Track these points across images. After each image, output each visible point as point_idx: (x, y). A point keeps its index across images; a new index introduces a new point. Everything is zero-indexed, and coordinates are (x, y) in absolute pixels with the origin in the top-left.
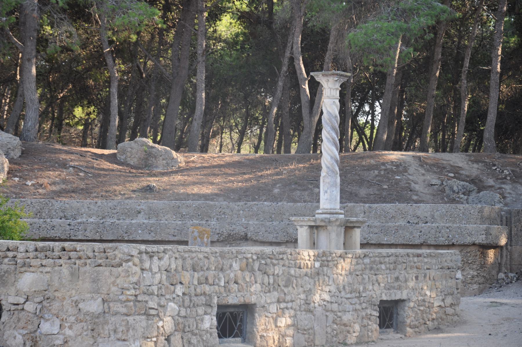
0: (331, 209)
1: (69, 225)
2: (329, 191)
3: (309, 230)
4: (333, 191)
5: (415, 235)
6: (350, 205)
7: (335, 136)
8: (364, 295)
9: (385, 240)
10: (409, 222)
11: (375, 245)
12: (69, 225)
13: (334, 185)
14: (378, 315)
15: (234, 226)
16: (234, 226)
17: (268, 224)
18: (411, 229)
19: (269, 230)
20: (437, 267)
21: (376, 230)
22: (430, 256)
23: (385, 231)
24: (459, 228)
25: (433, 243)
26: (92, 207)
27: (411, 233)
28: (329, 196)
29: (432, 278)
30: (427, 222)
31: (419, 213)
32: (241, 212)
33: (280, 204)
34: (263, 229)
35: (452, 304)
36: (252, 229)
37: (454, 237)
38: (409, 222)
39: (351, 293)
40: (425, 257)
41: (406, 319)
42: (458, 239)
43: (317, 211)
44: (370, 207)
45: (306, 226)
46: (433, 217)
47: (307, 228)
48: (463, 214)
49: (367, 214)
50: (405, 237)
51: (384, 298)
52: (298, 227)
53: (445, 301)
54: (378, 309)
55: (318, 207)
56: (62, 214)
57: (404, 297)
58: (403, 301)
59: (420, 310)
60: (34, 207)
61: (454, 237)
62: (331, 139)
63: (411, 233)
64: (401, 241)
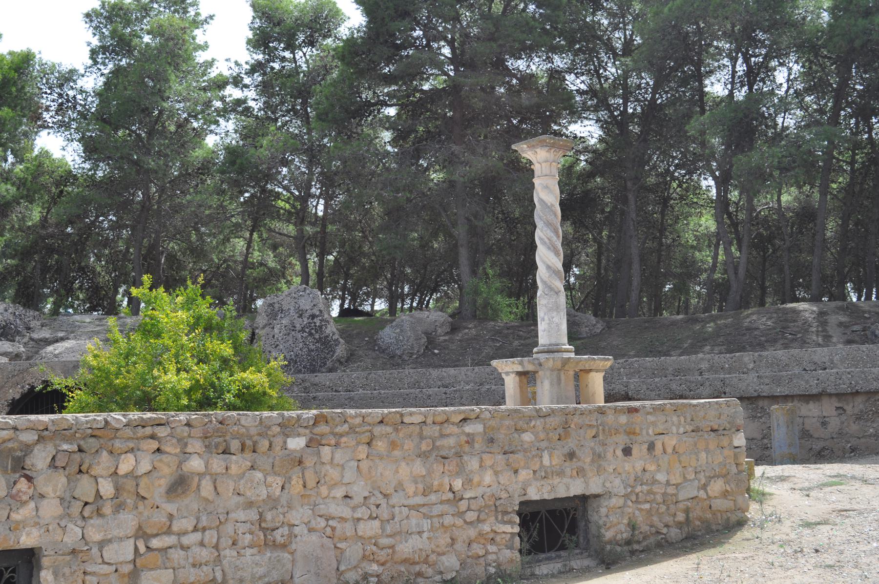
0: (550, 345)
1: (445, 393)
2: (546, 318)
3: (517, 378)
4: (553, 318)
5: (812, 384)
6: (737, 354)
7: (555, 238)
8: (467, 495)
9: (778, 391)
10: (805, 370)
11: (768, 397)
12: (445, 393)
13: (557, 308)
14: (517, 529)
15: (613, 386)
16: (613, 386)
17: (649, 380)
18: (807, 378)
19: (650, 388)
20: (682, 430)
21: (767, 381)
22: (655, 409)
23: (777, 381)
24: (862, 372)
25: (833, 391)
26: (469, 373)
27: (807, 382)
28: (552, 322)
29: (669, 450)
30: (825, 369)
31: (816, 358)
32: (622, 370)
33: (663, 358)
34: (645, 387)
35: (727, 491)
36: (632, 387)
37: (857, 383)
38: (805, 370)
39: (424, 494)
40: (648, 413)
41: (603, 531)
42: (862, 386)
43: (535, 350)
44: (760, 355)
45: (512, 372)
46: (832, 362)
47: (514, 375)
48: (867, 356)
49: (757, 363)
50: (800, 387)
51: (534, 494)
52: (504, 376)
53: (708, 488)
54: (517, 520)
55: (536, 344)
56: (440, 383)
57: (594, 488)
58: (597, 496)
59: (641, 510)
60: (412, 377)
61: (857, 383)
62: (546, 240)
63: (807, 382)
64: (796, 391)
